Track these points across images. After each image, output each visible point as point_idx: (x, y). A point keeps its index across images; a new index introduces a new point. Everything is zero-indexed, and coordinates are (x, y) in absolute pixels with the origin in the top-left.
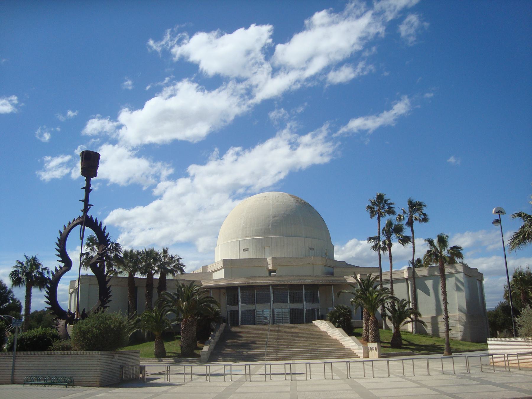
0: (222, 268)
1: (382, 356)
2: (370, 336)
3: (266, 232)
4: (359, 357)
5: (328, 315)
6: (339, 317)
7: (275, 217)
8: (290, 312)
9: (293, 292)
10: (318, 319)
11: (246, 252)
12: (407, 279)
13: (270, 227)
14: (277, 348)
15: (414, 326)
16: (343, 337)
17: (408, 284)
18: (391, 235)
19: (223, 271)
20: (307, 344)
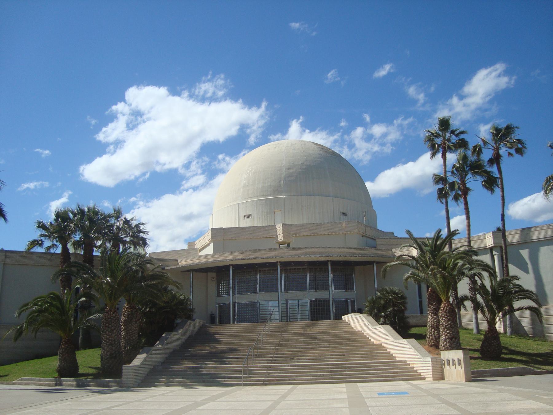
0: (211, 242)
1: (473, 376)
2: (443, 338)
3: (277, 190)
4: (424, 379)
5: (367, 304)
6: (385, 308)
7: (289, 169)
8: (311, 304)
9: (312, 271)
10: (354, 311)
11: (248, 219)
12: (491, 249)
13: (282, 182)
14: (272, 362)
15: (508, 323)
16: (392, 339)
17: (493, 257)
18: (466, 175)
19: (212, 245)
20: (327, 353)
